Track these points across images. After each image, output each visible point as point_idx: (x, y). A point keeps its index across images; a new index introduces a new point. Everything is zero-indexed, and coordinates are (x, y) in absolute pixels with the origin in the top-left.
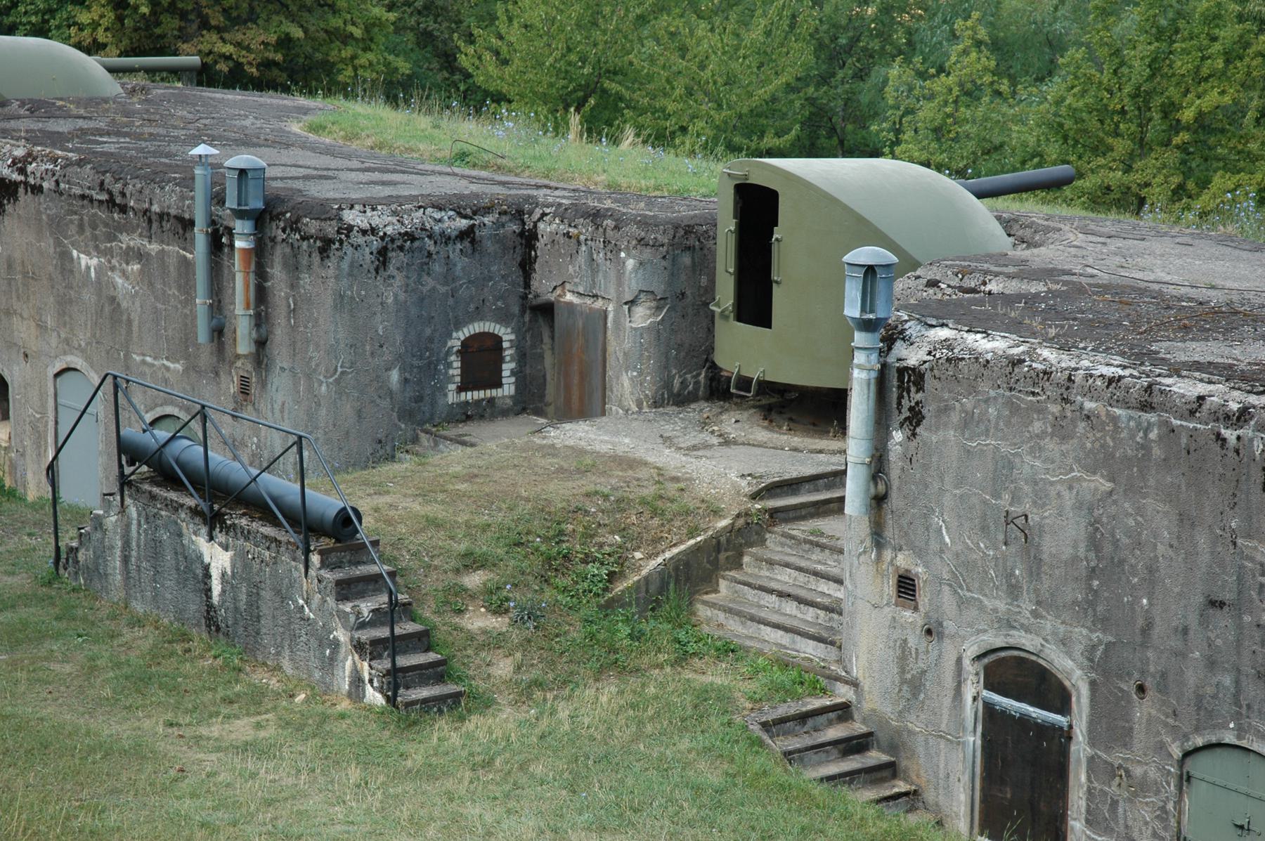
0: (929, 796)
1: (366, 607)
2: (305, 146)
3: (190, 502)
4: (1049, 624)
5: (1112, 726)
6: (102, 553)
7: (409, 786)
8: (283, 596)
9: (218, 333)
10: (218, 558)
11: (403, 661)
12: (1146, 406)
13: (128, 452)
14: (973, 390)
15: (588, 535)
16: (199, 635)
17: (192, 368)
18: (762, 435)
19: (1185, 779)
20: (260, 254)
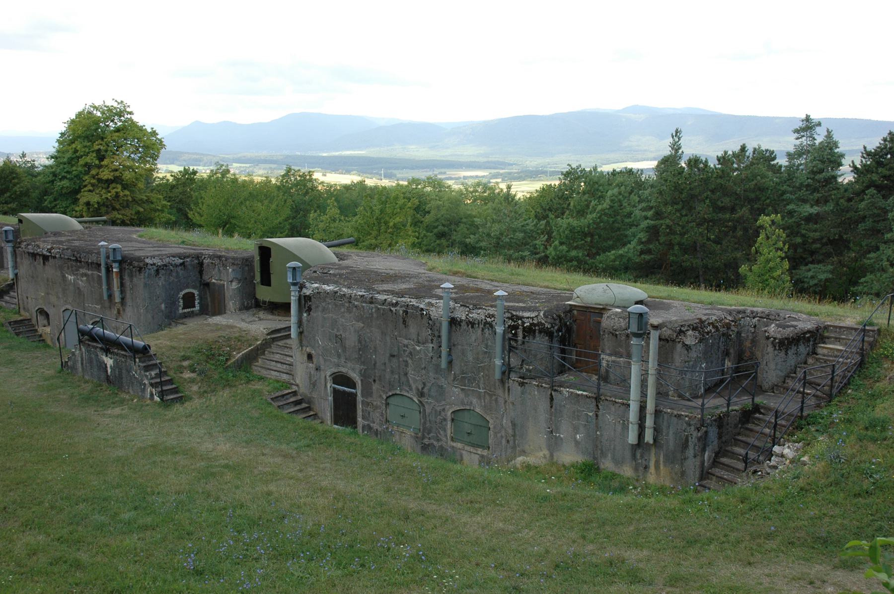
0: (320, 415)
1: (153, 373)
2: (136, 241)
3: (100, 346)
4: (349, 364)
5: (367, 392)
6: (75, 363)
7: (167, 424)
8: (129, 371)
9: (110, 296)
10: (109, 362)
11: (165, 388)
12: (371, 303)
13: (82, 333)
14: (325, 301)
15: (219, 348)
16: (105, 385)
17: (103, 307)
18: (270, 317)
19: (387, 404)
20: (121, 273)
